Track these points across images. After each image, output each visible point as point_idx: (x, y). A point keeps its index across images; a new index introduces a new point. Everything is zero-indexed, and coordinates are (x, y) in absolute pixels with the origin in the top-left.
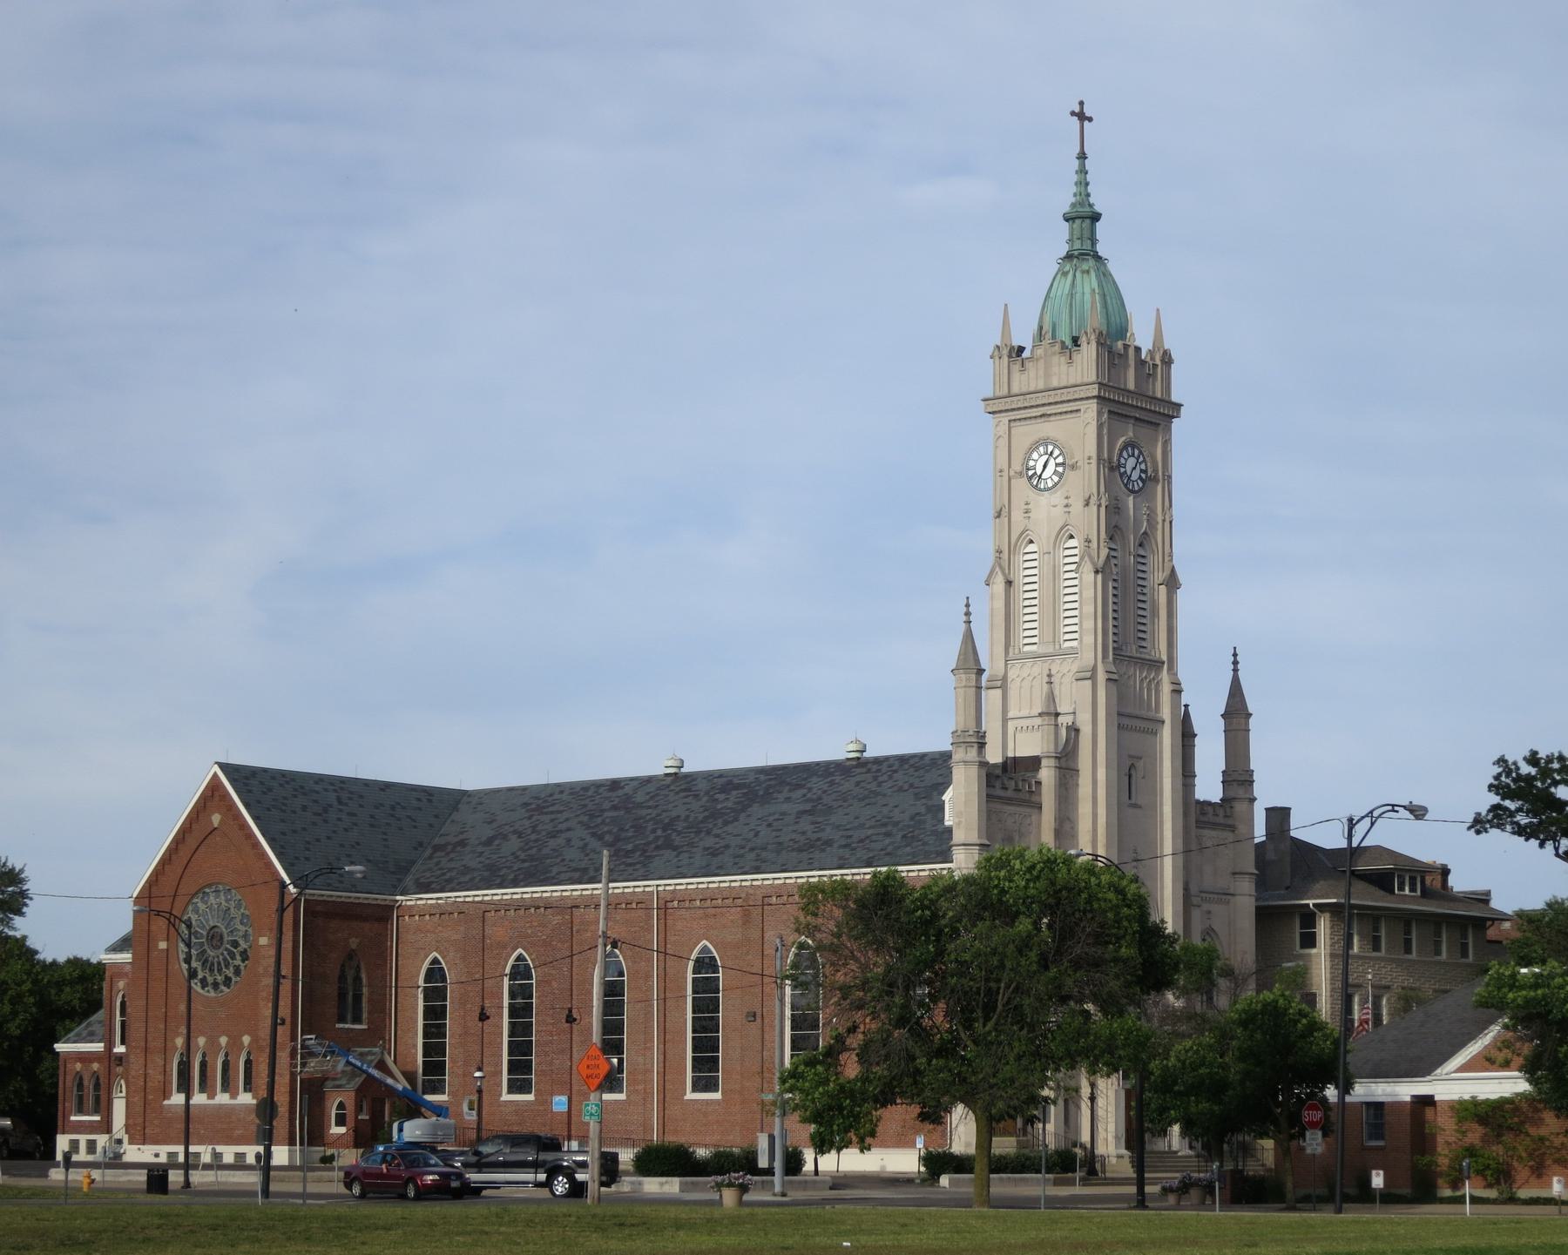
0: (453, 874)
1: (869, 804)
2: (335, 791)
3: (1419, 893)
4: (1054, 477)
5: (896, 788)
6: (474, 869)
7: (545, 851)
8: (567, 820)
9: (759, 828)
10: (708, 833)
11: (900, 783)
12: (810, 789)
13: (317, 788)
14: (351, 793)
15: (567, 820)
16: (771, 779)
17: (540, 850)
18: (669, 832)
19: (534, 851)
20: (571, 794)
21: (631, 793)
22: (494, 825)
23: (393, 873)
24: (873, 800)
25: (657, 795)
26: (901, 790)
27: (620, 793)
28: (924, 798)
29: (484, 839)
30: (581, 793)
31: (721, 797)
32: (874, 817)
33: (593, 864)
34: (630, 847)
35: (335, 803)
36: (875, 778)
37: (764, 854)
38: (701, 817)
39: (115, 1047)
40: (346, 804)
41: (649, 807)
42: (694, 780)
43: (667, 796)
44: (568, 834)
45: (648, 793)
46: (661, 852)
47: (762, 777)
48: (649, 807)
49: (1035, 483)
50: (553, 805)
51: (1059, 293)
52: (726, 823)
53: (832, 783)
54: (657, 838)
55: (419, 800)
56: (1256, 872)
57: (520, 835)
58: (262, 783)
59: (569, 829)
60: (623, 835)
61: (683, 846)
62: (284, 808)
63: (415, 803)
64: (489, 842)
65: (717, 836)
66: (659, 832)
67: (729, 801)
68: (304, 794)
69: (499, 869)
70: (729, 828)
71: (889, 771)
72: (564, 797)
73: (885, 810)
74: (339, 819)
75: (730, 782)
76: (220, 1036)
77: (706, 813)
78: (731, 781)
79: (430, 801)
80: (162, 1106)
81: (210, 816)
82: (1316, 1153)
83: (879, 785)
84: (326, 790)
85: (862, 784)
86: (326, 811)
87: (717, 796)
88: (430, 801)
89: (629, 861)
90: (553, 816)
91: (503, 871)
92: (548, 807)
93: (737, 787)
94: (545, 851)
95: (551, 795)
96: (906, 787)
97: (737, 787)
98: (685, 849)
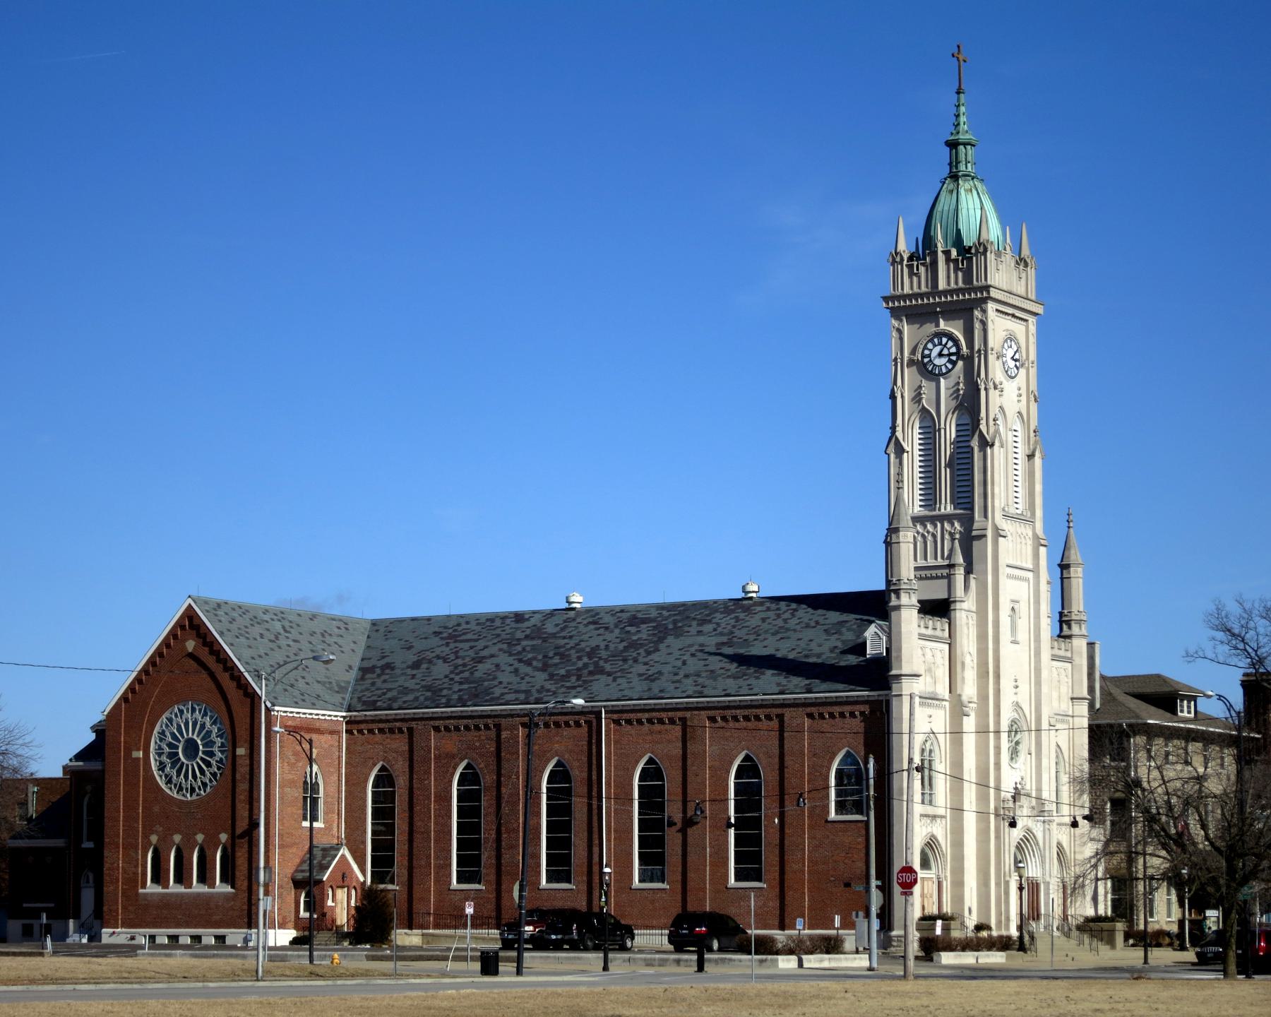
0: (394, 693)
1: (782, 638)
2: (279, 620)
3: (1192, 715)
4: (948, 365)
5: (803, 625)
6: (412, 690)
7: (477, 675)
8: (486, 647)
9: (685, 658)
10: (635, 660)
11: (806, 620)
12: (718, 624)
13: (266, 617)
14: (291, 622)
15: (486, 647)
16: (675, 615)
17: (472, 673)
18: (596, 659)
19: (466, 674)
20: (478, 624)
21: (539, 625)
22: (414, 651)
23: (338, 692)
24: (784, 635)
25: (566, 627)
26: (808, 626)
27: (526, 624)
28: (836, 633)
29: (410, 663)
30: (488, 624)
31: (633, 629)
32: (793, 649)
33: (533, 686)
34: (562, 672)
35: (282, 632)
36: (779, 616)
37: (700, 680)
38: (621, 646)
39: (82, 842)
40: (289, 632)
41: (564, 638)
42: (597, 614)
43: (576, 627)
44: (495, 660)
45: (557, 625)
46: (597, 677)
47: (665, 613)
48: (564, 638)
49: (930, 369)
50: (464, 634)
51: (946, 208)
52: (648, 653)
53: (737, 619)
54: (586, 665)
55: (339, 628)
56: (1089, 697)
57: (445, 660)
58: (226, 614)
59: (492, 656)
60: (550, 662)
61: (616, 672)
62: (247, 635)
63: (336, 630)
64: (416, 665)
65: (646, 664)
66: (585, 660)
67: (644, 632)
68: (258, 623)
69: (441, 690)
70: (655, 657)
71: (788, 610)
72: (473, 626)
73: (802, 644)
74: (289, 646)
75: (634, 617)
76: (196, 834)
77: (625, 644)
78: (634, 615)
79: (347, 629)
80: (137, 894)
81: (193, 640)
82: (1005, 1013)
83: (785, 621)
84: (273, 620)
85: (768, 621)
86: (277, 638)
87: (628, 629)
88: (347, 629)
89: (568, 684)
90: (472, 644)
91: (445, 692)
92: (460, 636)
93: (644, 621)
94: (477, 675)
95: (459, 625)
96: (813, 624)
97: (644, 621)
98: (619, 674)
